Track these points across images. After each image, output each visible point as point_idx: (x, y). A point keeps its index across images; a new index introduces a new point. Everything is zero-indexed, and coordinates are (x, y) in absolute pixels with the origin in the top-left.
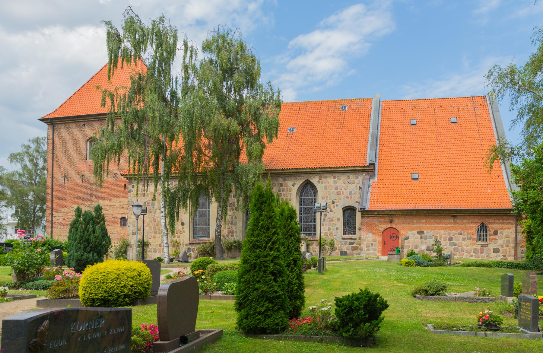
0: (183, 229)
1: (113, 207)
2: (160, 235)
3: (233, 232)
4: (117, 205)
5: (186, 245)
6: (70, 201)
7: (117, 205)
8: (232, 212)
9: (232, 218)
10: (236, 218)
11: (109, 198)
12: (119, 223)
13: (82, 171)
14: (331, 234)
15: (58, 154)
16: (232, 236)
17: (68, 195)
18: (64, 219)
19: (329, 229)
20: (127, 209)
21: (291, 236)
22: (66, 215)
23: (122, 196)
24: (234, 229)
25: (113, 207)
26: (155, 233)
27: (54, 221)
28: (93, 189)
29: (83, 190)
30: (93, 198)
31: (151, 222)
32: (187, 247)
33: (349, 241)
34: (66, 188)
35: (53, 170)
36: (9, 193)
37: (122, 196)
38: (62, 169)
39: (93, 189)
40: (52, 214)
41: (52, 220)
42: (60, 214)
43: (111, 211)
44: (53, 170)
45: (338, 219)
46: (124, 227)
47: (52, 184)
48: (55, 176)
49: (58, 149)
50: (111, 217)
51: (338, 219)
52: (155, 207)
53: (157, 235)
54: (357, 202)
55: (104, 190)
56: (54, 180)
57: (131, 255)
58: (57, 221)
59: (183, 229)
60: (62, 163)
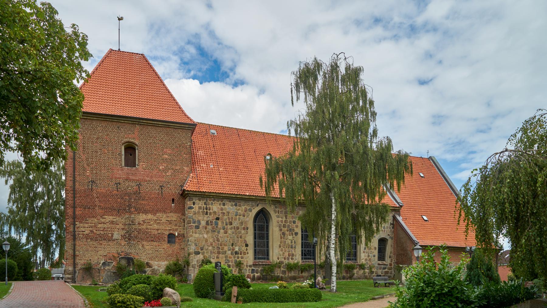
0: (247, 250)
1: (158, 221)
2: (224, 255)
3: (293, 255)
4: (164, 220)
5: (250, 266)
6: (101, 211)
7: (164, 220)
8: (291, 236)
9: (292, 242)
10: (295, 243)
11: (154, 212)
12: (166, 239)
13: (116, 178)
14: (370, 260)
15: (82, 154)
16: (292, 259)
17: (97, 203)
18: (92, 231)
19: (369, 256)
20: (176, 225)
21: (236, 253)
22: (95, 226)
23: (169, 211)
24: (294, 253)
25: (158, 221)
26: (219, 253)
27: (77, 233)
28: (133, 200)
29: (119, 200)
30: (133, 210)
31: (214, 241)
32: (251, 268)
33: (382, 266)
34: (95, 195)
35: (74, 172)
36: (55, 200)
37: (169, 211)
38: (88, 173)
39: (133, 200)
40: (74, 225)
41: (74, 231)
42: (86, 225)
43: (156, 226)
44: (74, 172)
45: (375, 248)
46: (173, 245)
47: (74, 188)
48: (78, 178)
49: (81, 148)
50: (156, 233)
51: (375, 248)
52: (219, 226)
53: (221, 255)
54: (389, 235)
55: (146, 202)
56: (77, 184)
57: (192, 275)
58: (82, 233)
59: (247, 250)
60: (88, 165)
